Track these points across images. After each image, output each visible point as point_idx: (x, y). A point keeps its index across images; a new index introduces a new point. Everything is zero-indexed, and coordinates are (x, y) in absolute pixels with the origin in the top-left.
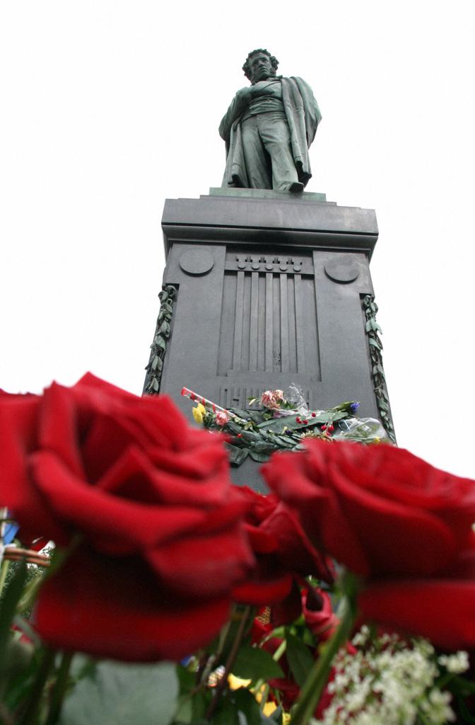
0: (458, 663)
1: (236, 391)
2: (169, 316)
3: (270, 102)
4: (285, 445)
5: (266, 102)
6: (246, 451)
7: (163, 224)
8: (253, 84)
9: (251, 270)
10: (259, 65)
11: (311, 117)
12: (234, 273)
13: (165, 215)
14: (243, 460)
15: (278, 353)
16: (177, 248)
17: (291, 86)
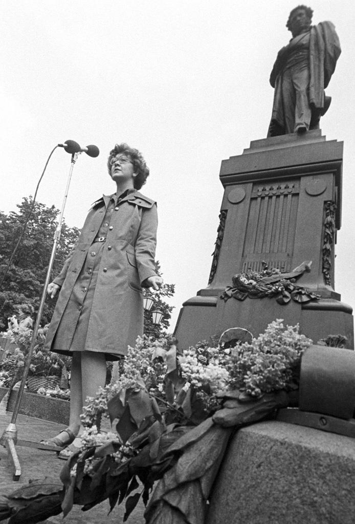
0: (231, 346)
1: (250, 264)
2: (222, 228)
3: (301, 53)
4: (263, 291)
5: (298, 55)
6: (246, 294)
7: (220, 176)
8: (295, 35)
9: (264, 196)
10: (299, 20)
11: (330, 55)
12: (256, 199)
13: (220, 174)
14: (245, 298)
15: (272, 243)
16: (227, 187)
17: (317, 36)
